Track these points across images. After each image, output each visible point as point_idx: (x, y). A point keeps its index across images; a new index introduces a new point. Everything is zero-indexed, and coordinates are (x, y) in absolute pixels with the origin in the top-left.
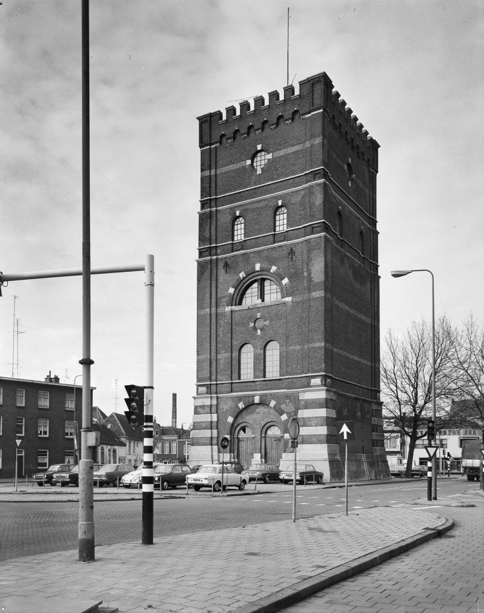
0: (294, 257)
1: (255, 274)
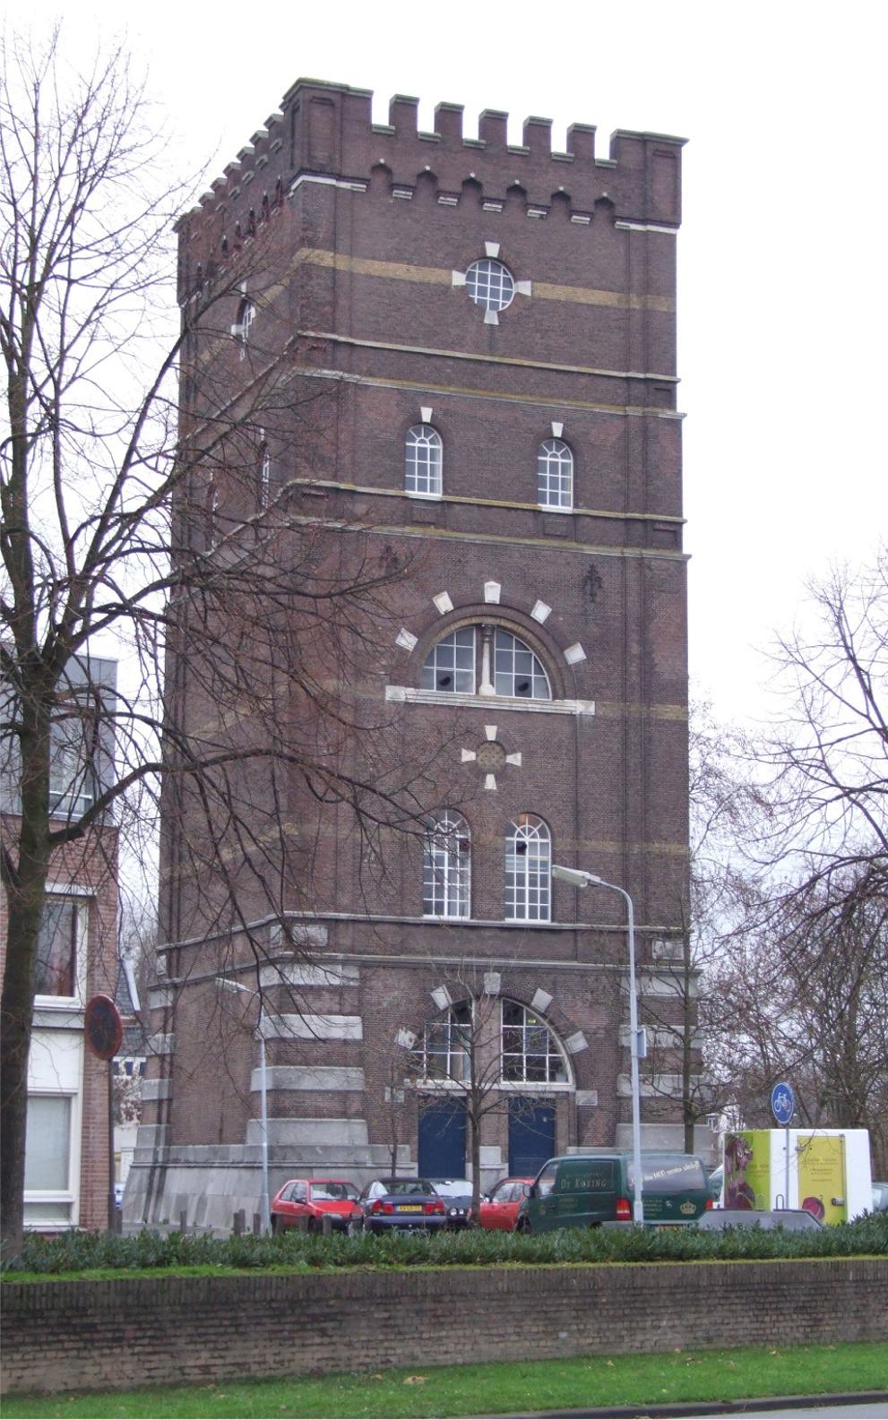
0: (599, 592)
1: (479, 609)
